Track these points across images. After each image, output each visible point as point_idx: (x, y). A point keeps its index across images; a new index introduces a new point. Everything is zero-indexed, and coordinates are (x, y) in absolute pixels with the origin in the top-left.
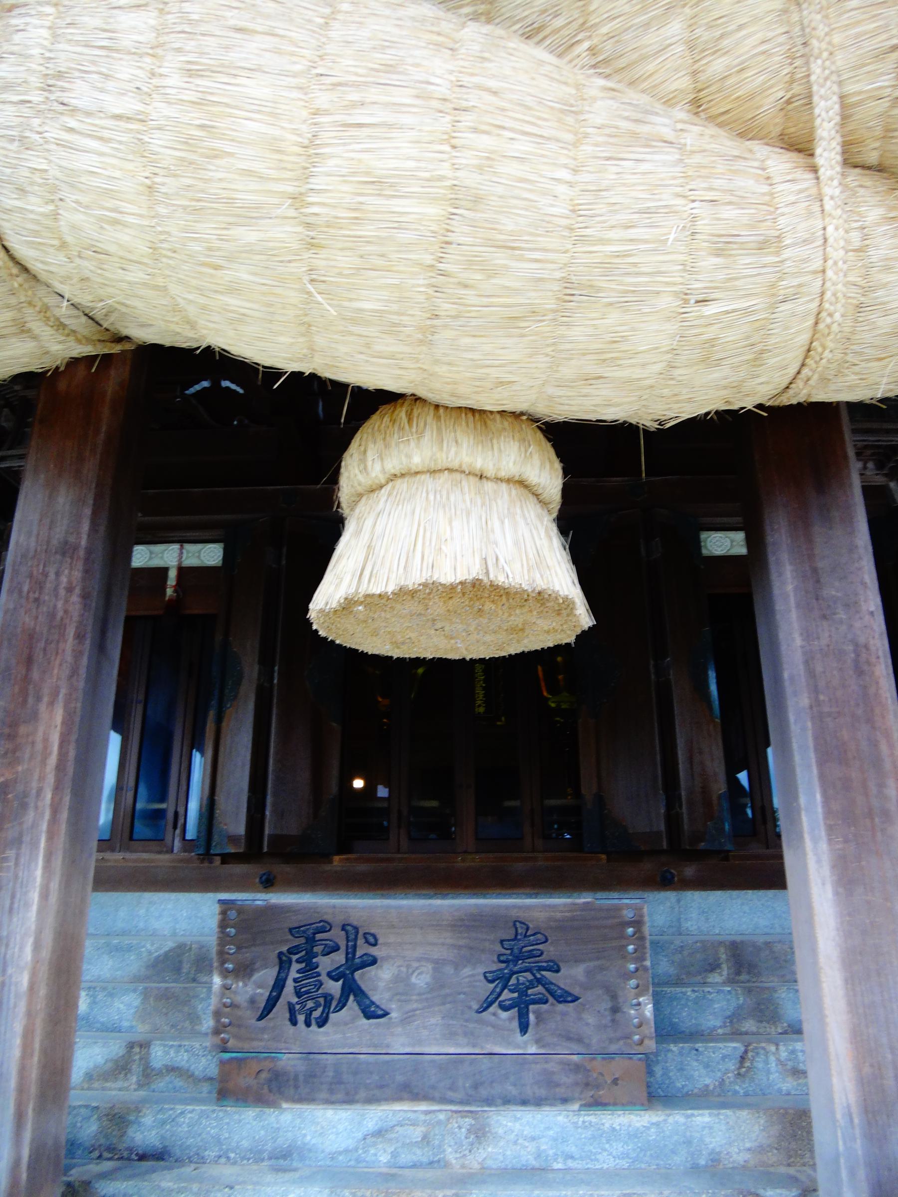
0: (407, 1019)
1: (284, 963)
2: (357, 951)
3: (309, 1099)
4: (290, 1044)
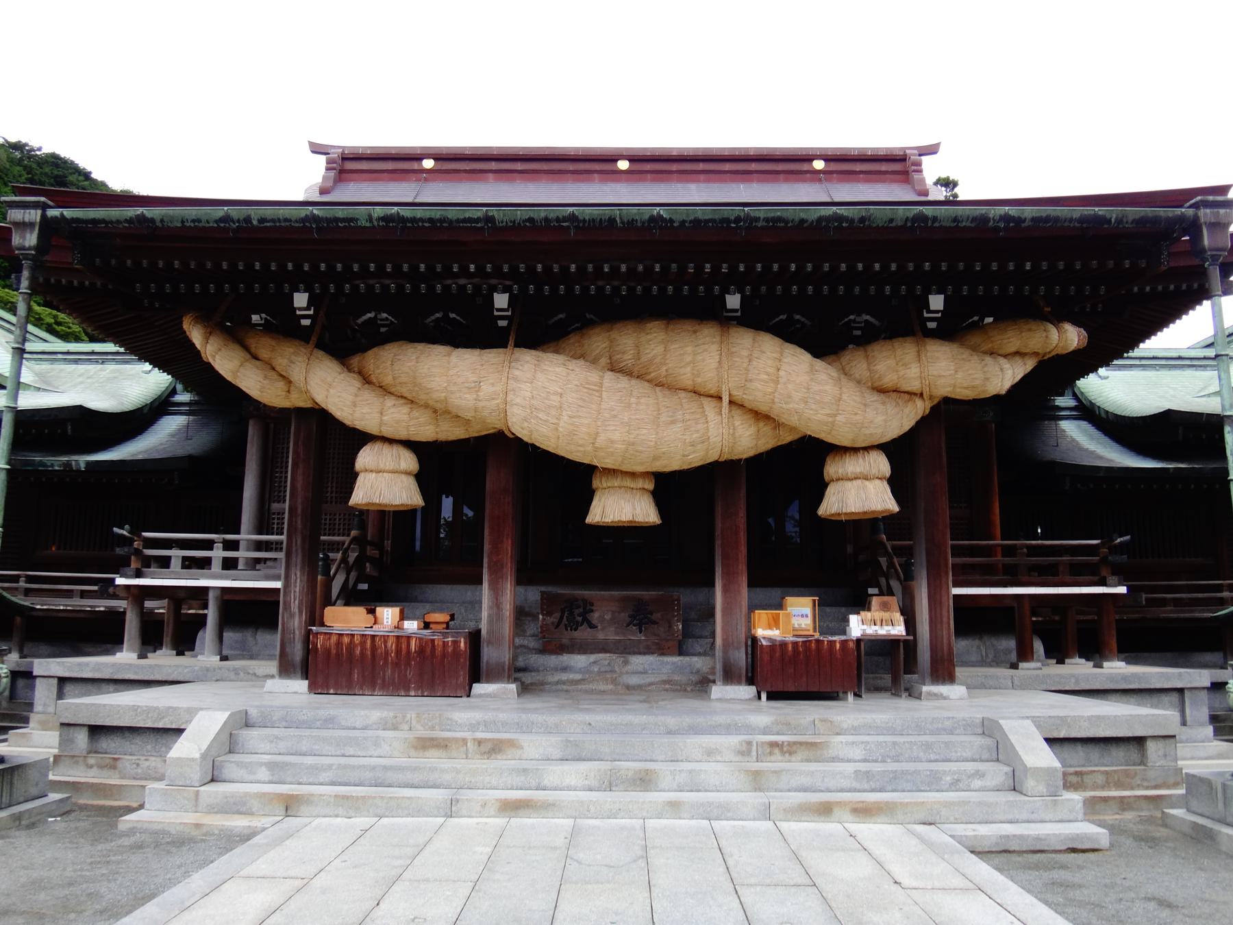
0: (603, 629)
1: (563, 612)
2: (587, 607)
3: (572, 652)
4: (566, 637)
